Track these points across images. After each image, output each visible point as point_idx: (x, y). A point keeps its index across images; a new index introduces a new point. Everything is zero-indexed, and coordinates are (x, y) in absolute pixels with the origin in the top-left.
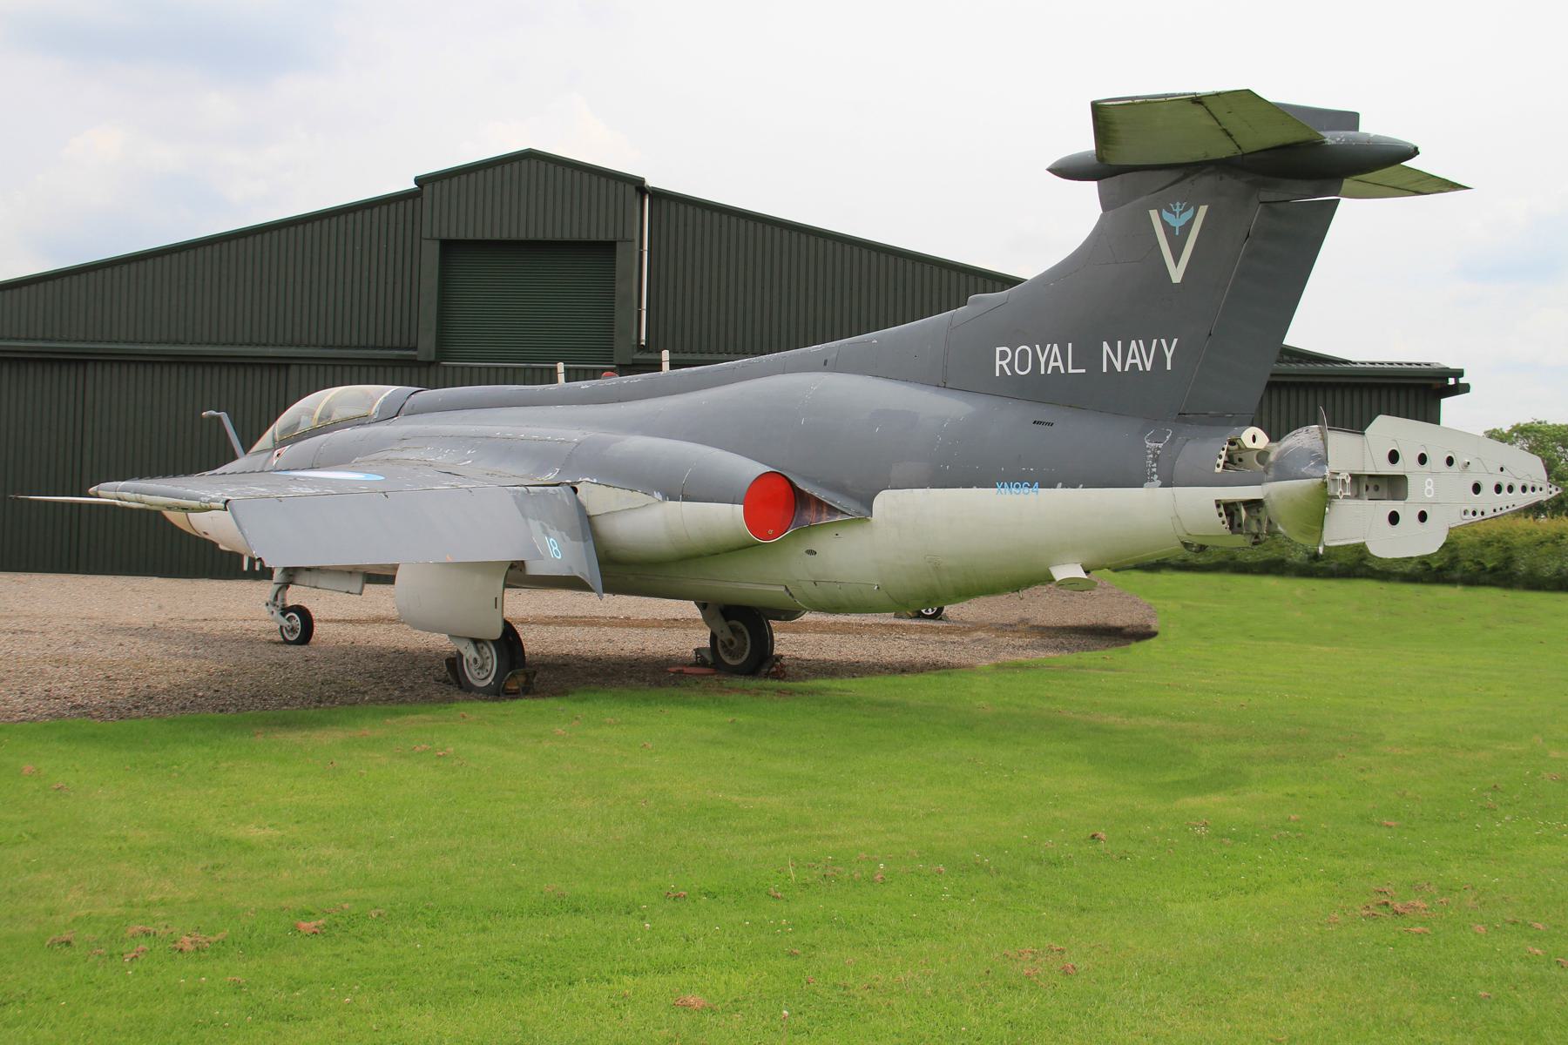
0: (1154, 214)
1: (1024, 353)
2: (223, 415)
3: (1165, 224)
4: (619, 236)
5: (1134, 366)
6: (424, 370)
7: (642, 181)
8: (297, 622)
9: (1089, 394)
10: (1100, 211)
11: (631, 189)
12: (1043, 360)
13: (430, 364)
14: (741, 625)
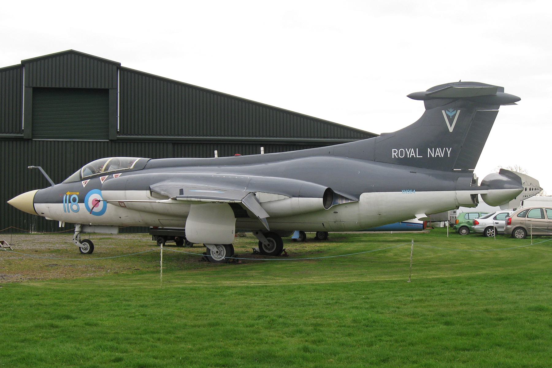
0: (443, 112)
1: (402, 152)
2: (40, 168)
3: (447, 115)
4: (110, 87)
5: (438, 156)
6: (26, 143)
7: (120, 64)
8: (88, 245)
9: (423, 163)
10: (425, 110)
11: (115, 68)
12: (408, 154)
13: (28, 140)
14: (272, 239)
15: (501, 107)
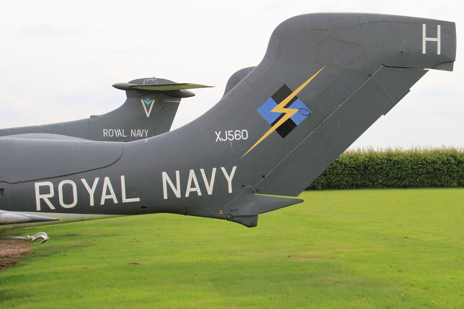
0: (142, 100)
1: (111, 131)
3: (145, 103)
12: (116, 133)
15: (182, 99)
